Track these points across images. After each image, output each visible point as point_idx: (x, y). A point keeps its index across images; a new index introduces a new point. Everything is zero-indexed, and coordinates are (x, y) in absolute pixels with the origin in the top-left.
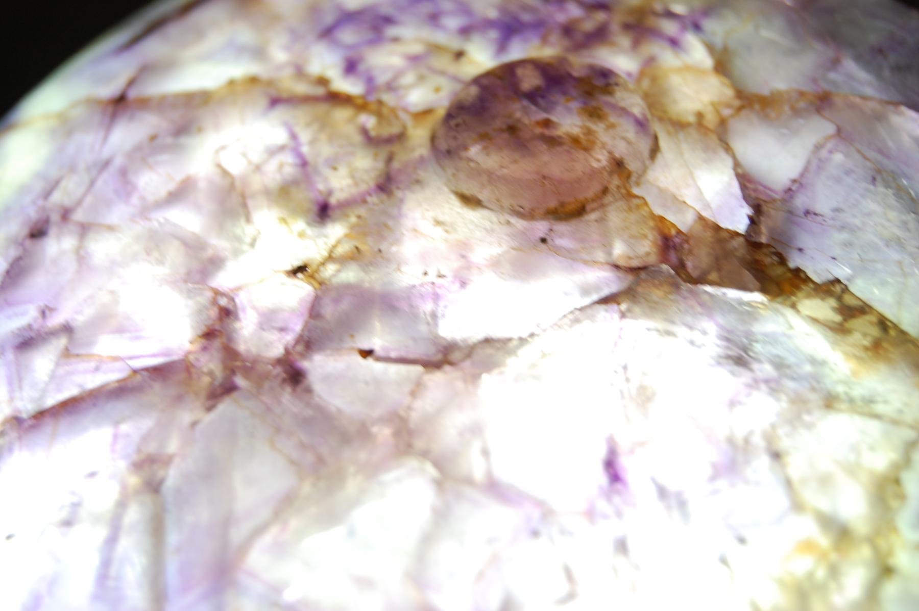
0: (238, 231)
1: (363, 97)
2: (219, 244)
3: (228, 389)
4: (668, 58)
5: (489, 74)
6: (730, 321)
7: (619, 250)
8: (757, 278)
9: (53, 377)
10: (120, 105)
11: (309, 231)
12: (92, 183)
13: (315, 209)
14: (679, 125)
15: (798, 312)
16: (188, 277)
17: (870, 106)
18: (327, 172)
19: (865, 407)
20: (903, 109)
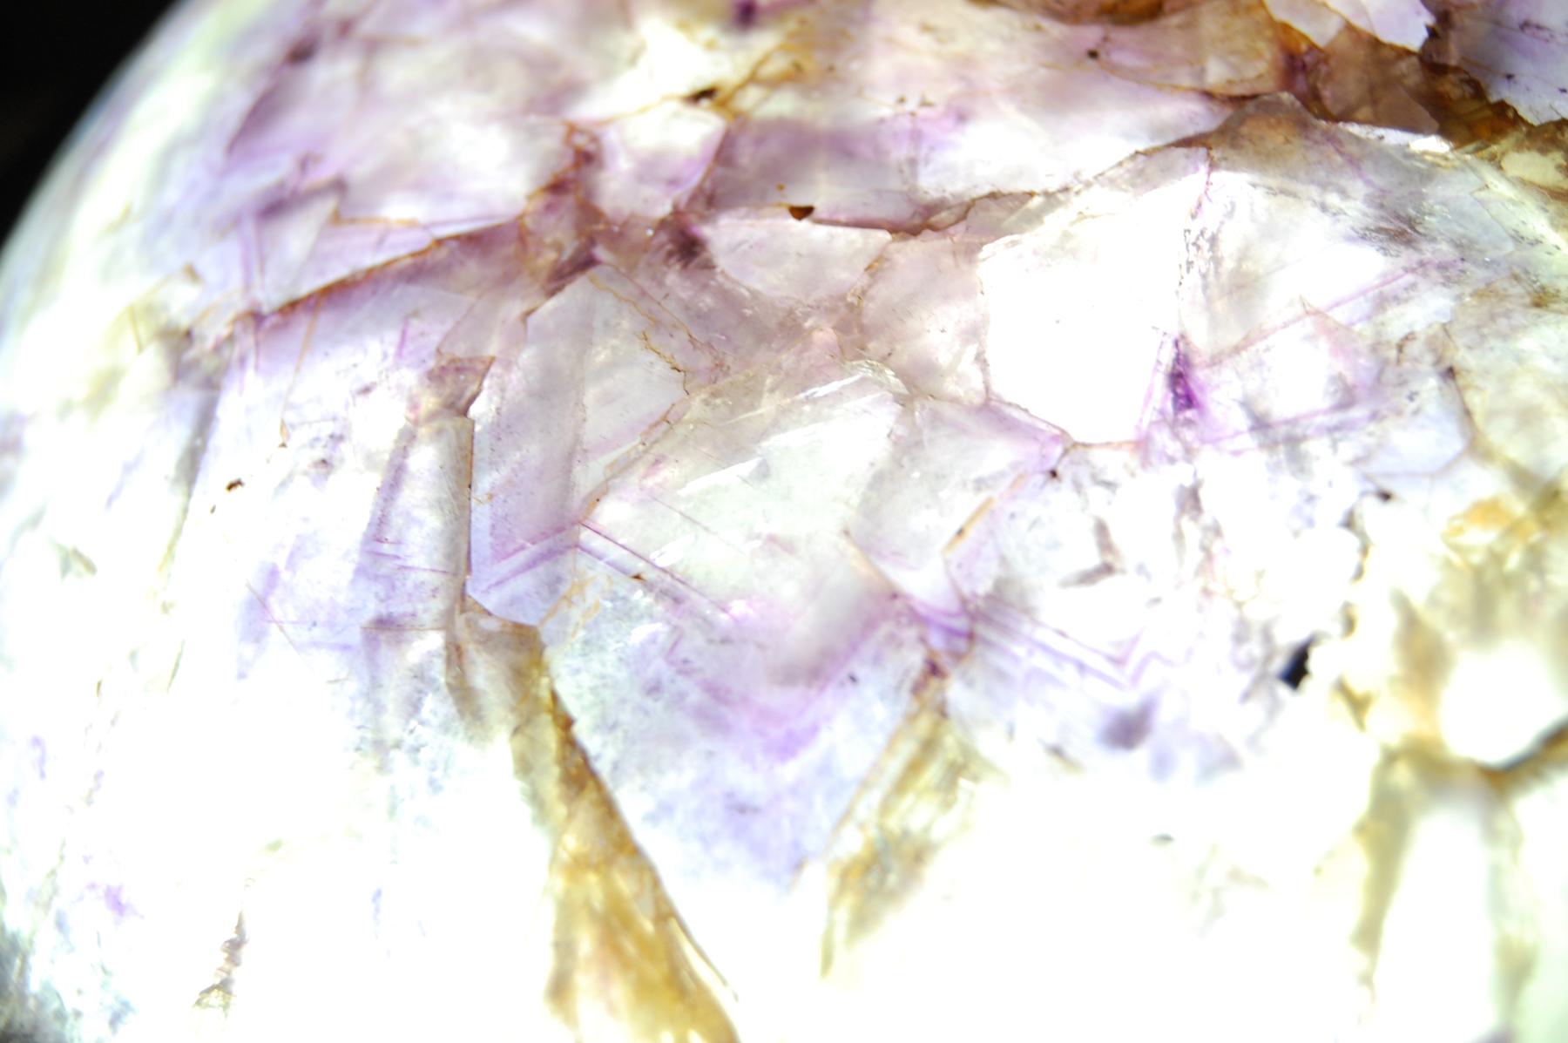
2: (582, 64)
3: (583, 263)
7: (1216, 73)
8: (1434, 115)
15: (1500, 168)
16: (531, 106)
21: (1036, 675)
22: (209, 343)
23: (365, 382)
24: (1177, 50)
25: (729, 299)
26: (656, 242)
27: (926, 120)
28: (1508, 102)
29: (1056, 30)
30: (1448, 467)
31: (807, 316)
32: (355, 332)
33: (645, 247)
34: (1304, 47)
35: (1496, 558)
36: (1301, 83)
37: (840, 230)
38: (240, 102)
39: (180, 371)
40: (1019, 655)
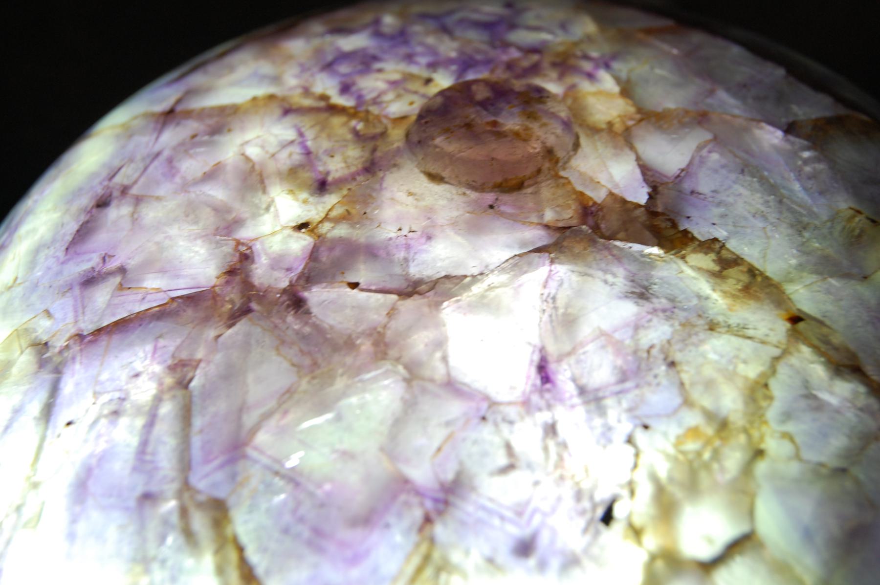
1: (355, 108)
2: (241, 210)
3: (245, 311)
4: (586, 86)
5: (449, 89)
6: (633, 268)
7: (549, 216)
9: (109, 305)
10: (170, 116)
11: (311, 199)
12: (146, 169)
13: (316, 184)
14: (594, 130)
16: (217, 231)
17: (739, 122)
18: (325, 158)
19: (740, 331)
20: (763, 125)
21: (480, 522)
22: (57, 350)
23: (138, 371)
24: (531, 205)
25: (319, 329)
26: (281, 300)
27: (411, 239)
28: (690, 230)
29: (473, 195)
30: (675, 411)
31: (358, 338)
32: (131, 345)
33: (275, 303)
34: (591, 203)
35: (699, 454)
36: (591, 220)
37: (372, 294)
38: (73, 227)
39: (42, 364)
40: (467, 508)
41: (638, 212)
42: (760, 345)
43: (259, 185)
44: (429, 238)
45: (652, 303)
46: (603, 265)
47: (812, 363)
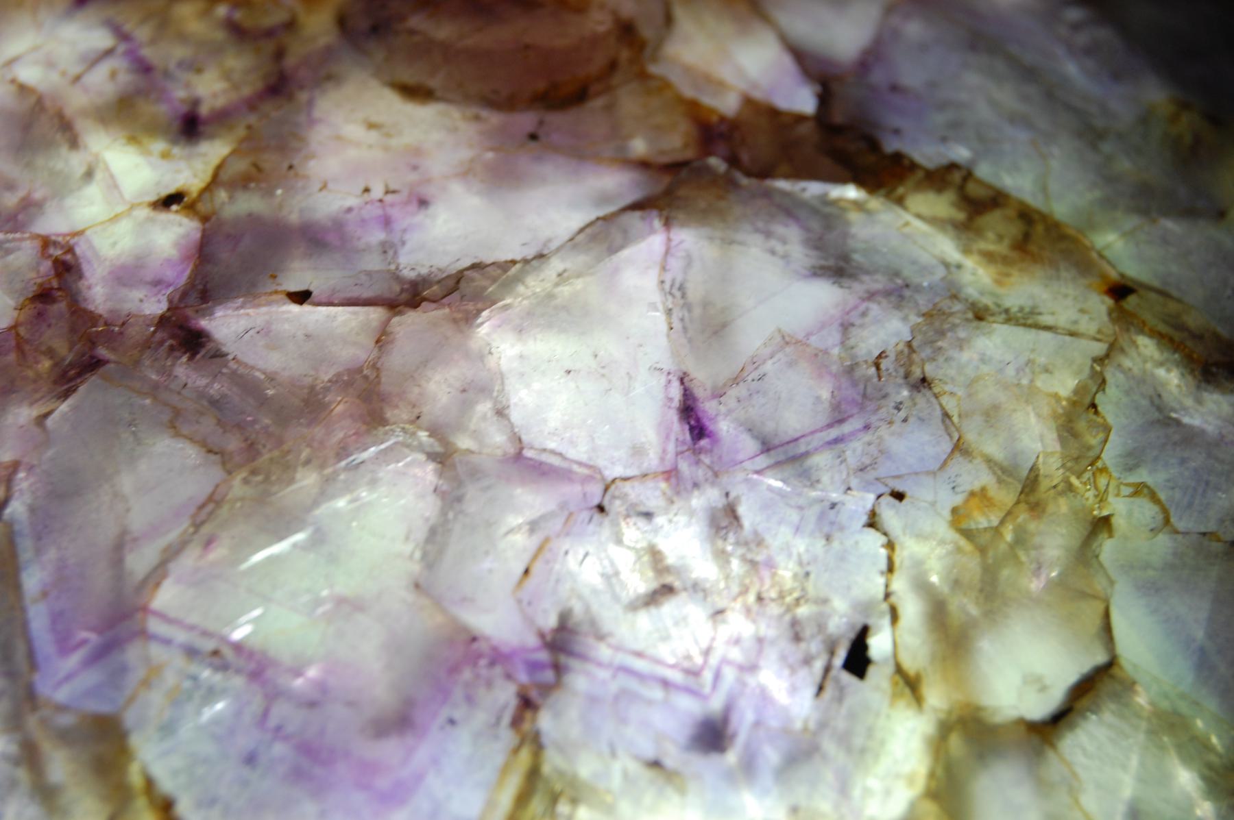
0: (59, 165)
3: (92, 365)
7: (639, 147)
11: (176, 151)
13: (176, 125)
19: (1026, 319)
25: (249, 386)
26: (159, 336)
27: (392, 205)
29: (494, 119)
41: (805, 129)
42: (1068, 338)
43: (58, 136)
44: (423, 203)
45: (862, 282)
46: (760, 224)
47: (1161, 364)
